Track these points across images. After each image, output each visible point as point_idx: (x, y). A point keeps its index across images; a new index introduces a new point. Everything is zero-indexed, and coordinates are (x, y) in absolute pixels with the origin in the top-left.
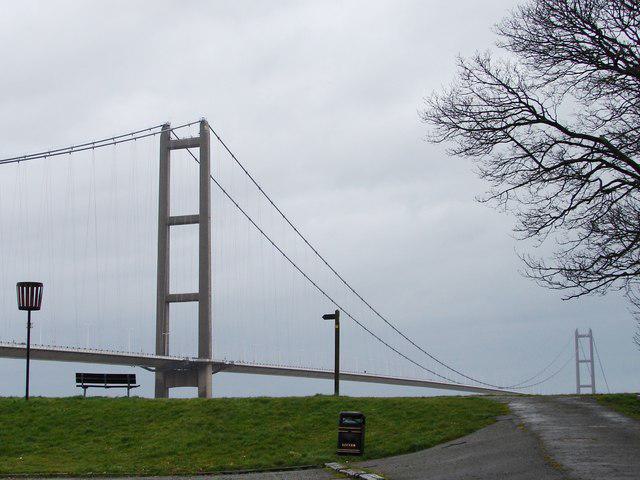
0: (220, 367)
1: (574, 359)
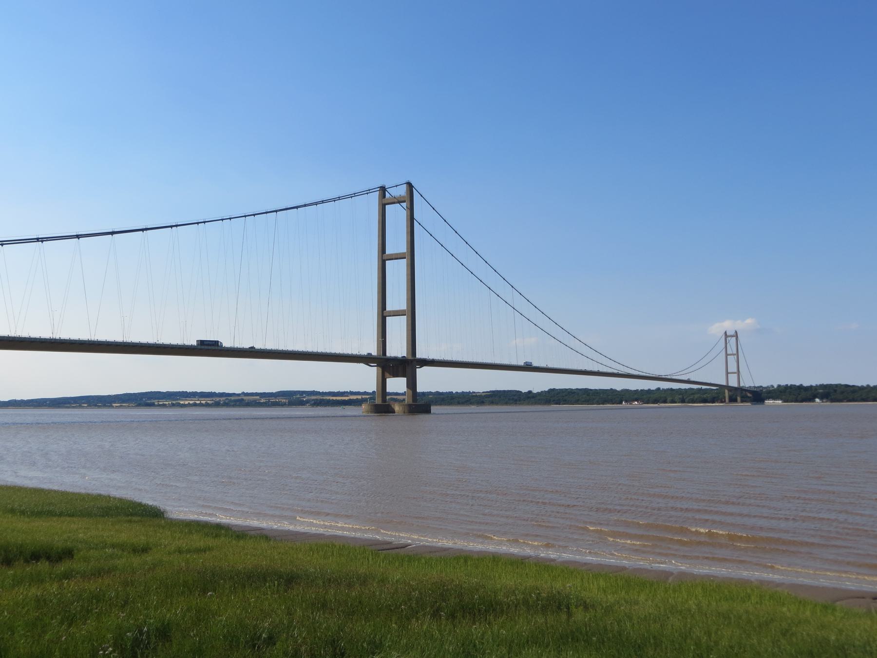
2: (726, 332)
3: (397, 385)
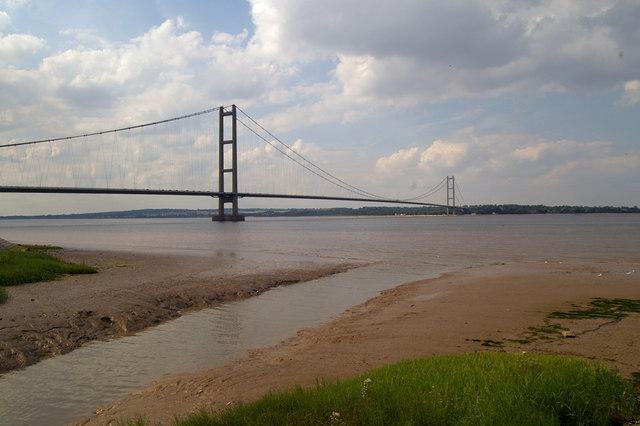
0: (243, 195)
3: (228, 206)
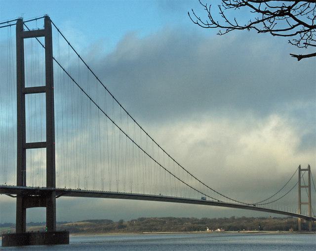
1: (298, 185)
2: (300, 166)
3: (36, 215)
